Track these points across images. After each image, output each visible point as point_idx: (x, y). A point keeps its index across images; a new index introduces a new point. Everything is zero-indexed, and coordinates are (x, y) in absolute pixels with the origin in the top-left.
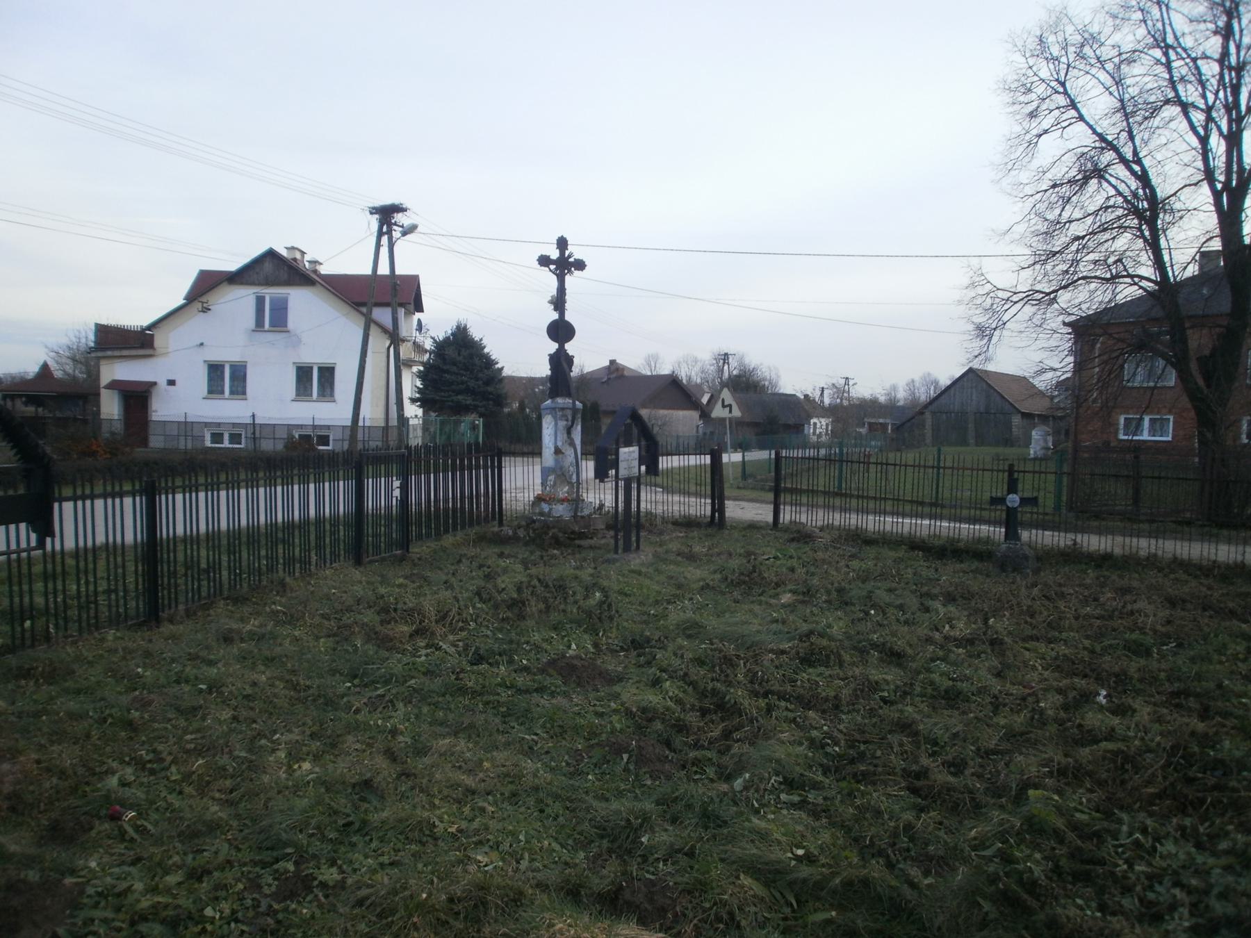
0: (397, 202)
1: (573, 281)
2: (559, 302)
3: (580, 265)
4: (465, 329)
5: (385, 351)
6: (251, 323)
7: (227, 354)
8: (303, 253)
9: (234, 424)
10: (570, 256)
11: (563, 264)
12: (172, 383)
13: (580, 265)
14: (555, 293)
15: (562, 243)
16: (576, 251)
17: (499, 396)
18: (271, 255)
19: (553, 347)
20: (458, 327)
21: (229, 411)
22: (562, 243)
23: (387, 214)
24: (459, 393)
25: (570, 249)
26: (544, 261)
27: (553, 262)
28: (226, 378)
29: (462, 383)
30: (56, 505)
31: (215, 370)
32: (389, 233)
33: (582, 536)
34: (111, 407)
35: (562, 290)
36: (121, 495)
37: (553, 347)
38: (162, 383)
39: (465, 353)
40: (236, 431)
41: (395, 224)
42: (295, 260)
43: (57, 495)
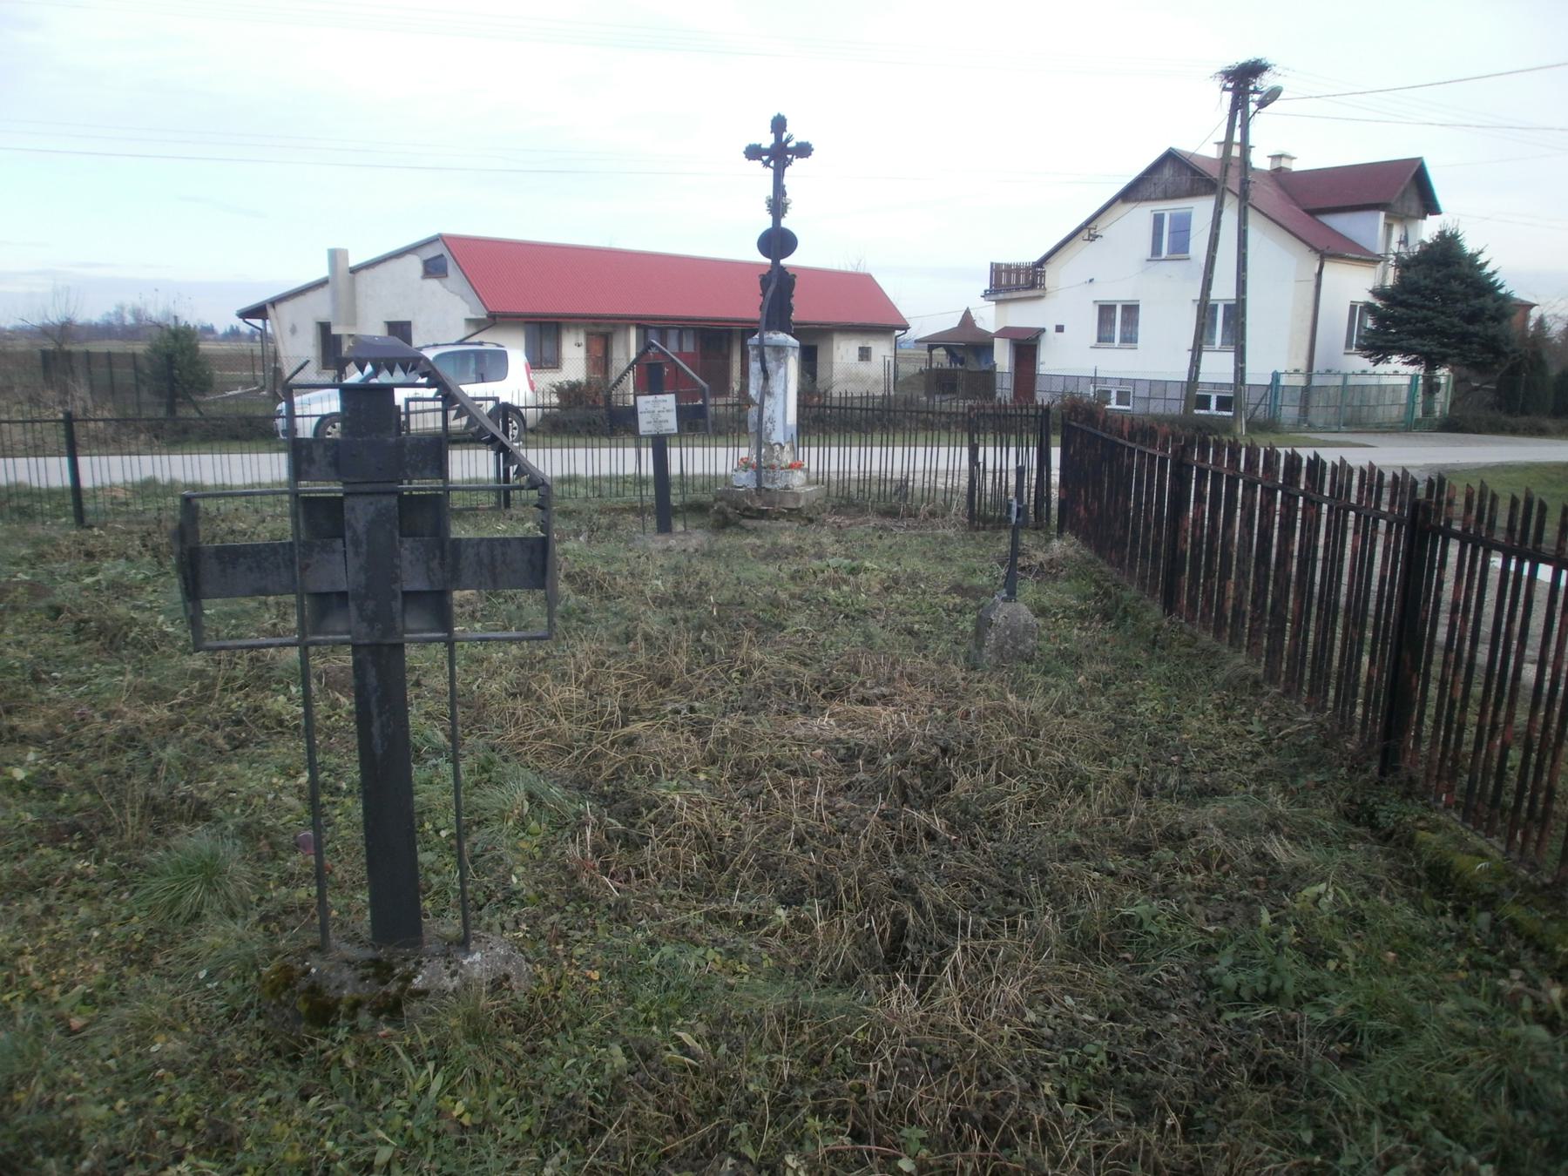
1: (796, 171)
2: (778, 205)
4: (1455, 237)
5: (1313, 278)
6: (1146, 250)
7: (1118, 294)
9: (1121, 380)
10: (788, 141)
11: (780, 153)
12: (1060, 329)
13: (804, 150)
15: (779, 124)
16: (796, 133)
18: (1171, 158)
21: (1116, 364)
22: (779, 124)
26: (753, 152)
27: (766, 152)
28: (1119, 321)
29: (1425, 320)
31: (1106, 311)
34: (1003, 357)
35: (779, 189)
38: (1051, 329)
40: (1124, 388)
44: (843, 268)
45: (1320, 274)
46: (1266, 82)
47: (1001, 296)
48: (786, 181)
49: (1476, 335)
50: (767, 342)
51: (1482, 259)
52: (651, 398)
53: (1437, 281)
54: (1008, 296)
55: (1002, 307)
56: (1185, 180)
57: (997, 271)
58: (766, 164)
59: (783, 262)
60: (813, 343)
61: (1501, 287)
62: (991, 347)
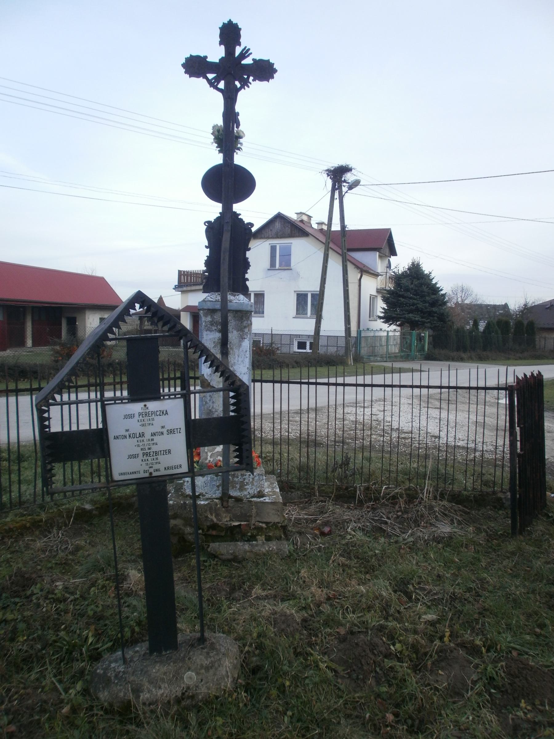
0: (344, 164)
1: (252, 99)
2: (227, 137)
3: (264, 70)
4: (418, 265)
5: (357, 281)
6: (267, 264)
8: (309, 217)
11: (232, 69)
13: (264, 70)
14: (220, 122)
15: (230, 34)
16: (255, 45)
17: (442, 314)
18: (279, 217)
19: (214, 210)
20: (413, 264)
22: (230, 34)
23: (338, 175)
24: (411, 312)
25: (246, 41)
26: (196, 66)
29: (413, 305)
30: (161, 382)
32: (340, 188)
33: (232, 534)
35: (230, 116)
36: (17, 392)
37: (214, 210)
39: (416, 282)
41: (345, 181)
42: (302, 221)
43: (161, 377)
44: (83, 273)
45: (360, 280)
46: (349, 177)
47: (185, 289)
48: (238, 108)
49: (435, 313)
50: (231, 306)
51: (432, 276)
52: (137, 407)
53: (415, 285)
54: (189, 288)
55: (185, 295)
56: (288, 230)
57: (181, 274)
58: (213, 84)
59: (237, 207)
60: (74, 316)
61: (442, 290)
62: (179, 317)
